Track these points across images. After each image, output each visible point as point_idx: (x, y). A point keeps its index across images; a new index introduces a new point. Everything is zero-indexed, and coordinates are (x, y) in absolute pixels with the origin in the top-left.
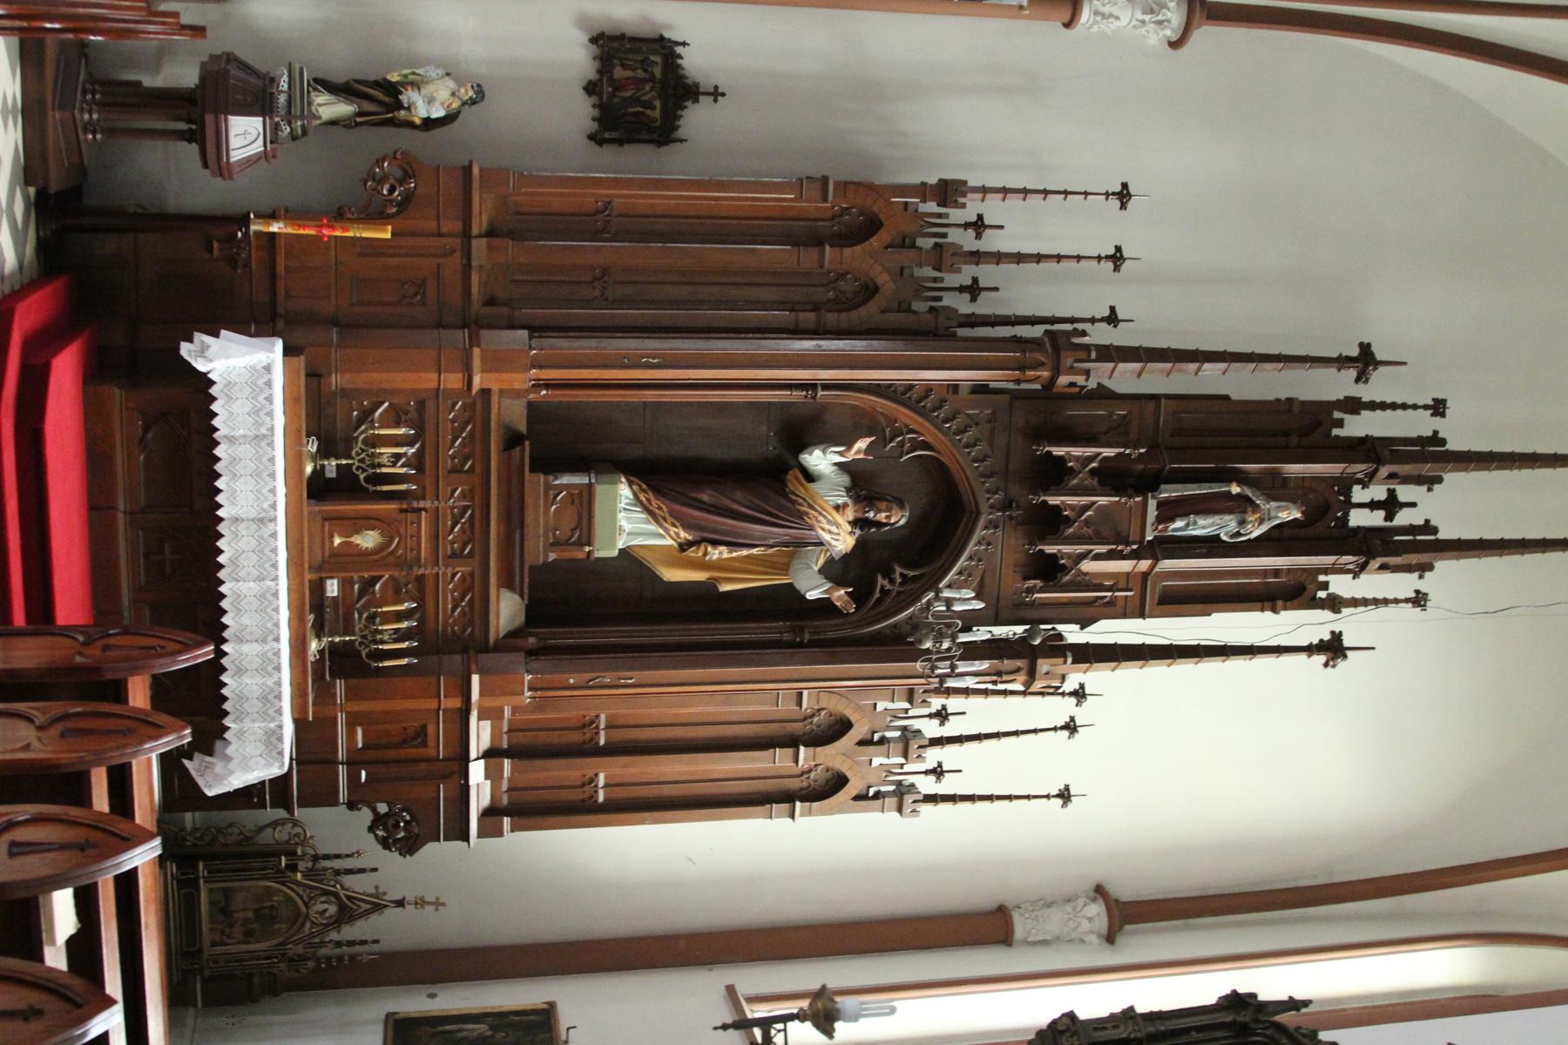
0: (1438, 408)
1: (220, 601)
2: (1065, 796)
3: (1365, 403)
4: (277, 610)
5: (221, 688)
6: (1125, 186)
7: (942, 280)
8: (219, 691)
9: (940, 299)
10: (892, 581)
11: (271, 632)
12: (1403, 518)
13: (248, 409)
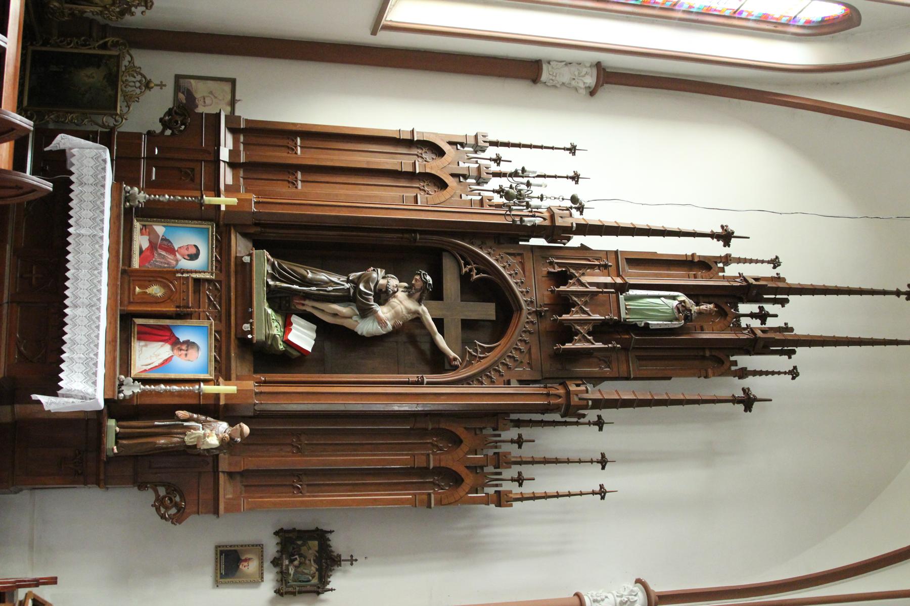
0: (775, 263)
1: (64, 327)
2: (572, 150)
3: (734, 258)
4: (98, 318)
5: (67, 255)
6: (603, 455)
7: (499, 436)
8: (64, 283)
9: (500, 447)
10: (471, 270)
11: (92, 359)
12: (771, 323)
13: (91, 173)
